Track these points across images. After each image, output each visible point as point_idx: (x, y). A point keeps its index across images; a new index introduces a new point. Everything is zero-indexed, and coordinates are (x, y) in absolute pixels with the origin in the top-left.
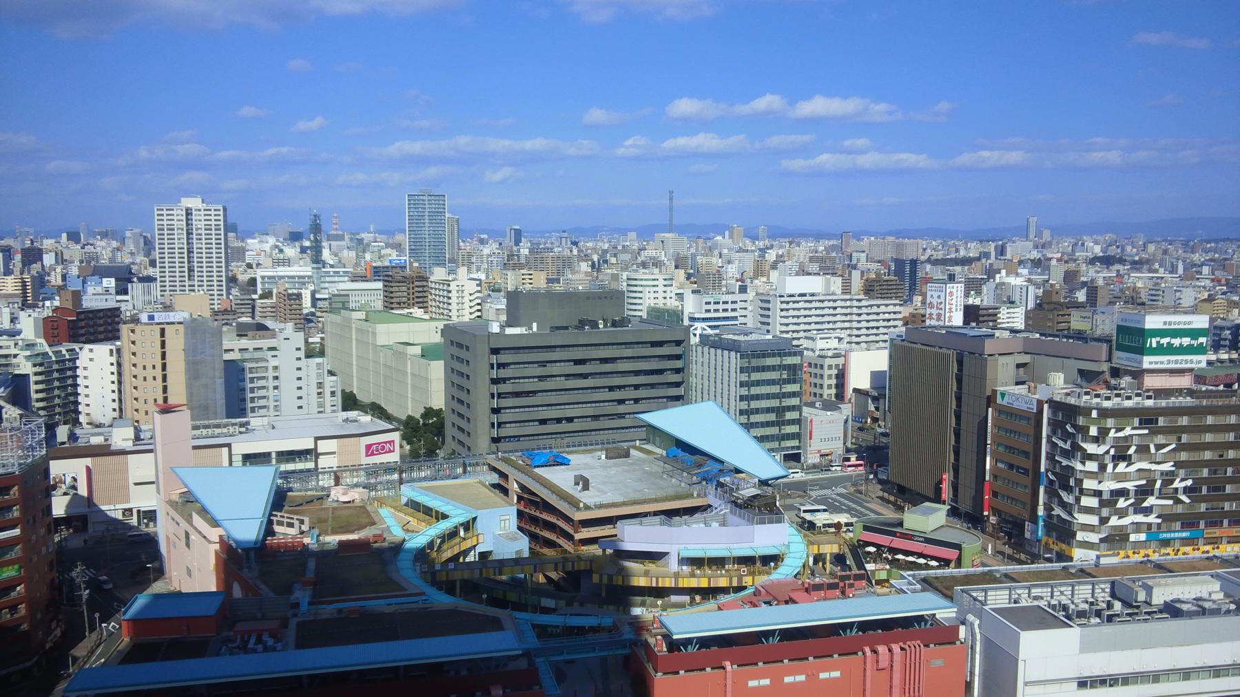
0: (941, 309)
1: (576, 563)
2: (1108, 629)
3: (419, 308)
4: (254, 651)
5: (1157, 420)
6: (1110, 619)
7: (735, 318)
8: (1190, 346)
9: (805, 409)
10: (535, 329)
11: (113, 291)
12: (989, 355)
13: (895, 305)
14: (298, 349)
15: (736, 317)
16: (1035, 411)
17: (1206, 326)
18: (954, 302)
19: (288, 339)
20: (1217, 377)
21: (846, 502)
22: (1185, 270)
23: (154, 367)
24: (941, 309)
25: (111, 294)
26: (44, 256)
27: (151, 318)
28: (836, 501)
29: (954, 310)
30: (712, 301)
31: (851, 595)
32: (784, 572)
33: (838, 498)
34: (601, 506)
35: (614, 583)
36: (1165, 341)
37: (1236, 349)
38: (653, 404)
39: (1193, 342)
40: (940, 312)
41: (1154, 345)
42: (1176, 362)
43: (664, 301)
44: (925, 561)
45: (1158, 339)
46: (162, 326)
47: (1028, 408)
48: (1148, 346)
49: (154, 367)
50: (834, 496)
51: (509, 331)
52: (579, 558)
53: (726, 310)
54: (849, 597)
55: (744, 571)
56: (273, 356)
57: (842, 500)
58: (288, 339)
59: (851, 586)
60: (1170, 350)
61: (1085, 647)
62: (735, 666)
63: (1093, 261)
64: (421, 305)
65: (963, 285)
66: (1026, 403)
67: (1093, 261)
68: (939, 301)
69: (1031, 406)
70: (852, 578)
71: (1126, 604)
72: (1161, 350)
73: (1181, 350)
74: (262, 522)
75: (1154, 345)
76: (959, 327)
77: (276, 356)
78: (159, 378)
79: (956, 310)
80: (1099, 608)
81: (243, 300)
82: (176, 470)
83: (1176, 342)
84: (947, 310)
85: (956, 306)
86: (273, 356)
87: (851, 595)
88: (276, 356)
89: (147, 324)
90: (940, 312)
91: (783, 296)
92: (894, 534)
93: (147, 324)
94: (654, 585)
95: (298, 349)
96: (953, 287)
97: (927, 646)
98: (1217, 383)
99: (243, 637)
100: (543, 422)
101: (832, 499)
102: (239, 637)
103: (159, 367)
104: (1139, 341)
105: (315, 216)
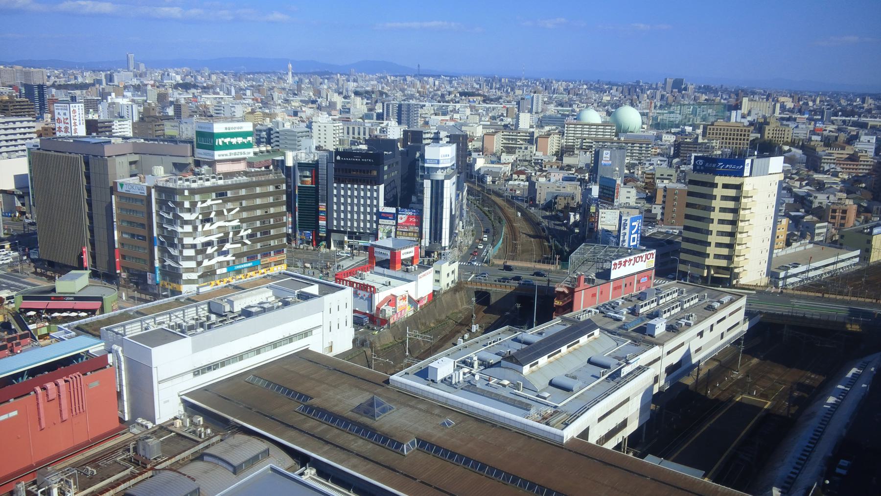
0: (68, 123)
2: (209, 333)
5: (226, 193)
12: (109, 157)
16: (146, 195)
24: (68, 123)
29: (78, 124)
39: (244, 140)
40: (67, 125)
41: (221, 143)
42: (235, 154)
45: (223, 139)
47: (140, 193)
60: (230, 146)
63: (176, 86)
69: (143, 191)
71: (219, 315)
72: (226, 147)
83: (234, 141)
84: (72, 124)
85: (80, 120)
90: (67, 125)
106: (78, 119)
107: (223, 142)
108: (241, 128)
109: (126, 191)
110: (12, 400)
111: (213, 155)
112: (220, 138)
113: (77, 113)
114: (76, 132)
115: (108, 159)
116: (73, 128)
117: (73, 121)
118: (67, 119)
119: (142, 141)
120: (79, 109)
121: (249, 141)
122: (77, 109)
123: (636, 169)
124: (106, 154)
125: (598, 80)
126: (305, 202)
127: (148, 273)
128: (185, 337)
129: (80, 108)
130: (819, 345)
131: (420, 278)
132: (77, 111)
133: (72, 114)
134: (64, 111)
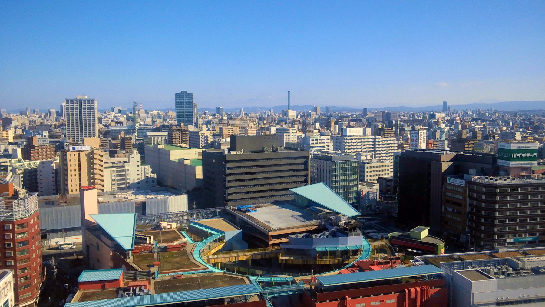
0: (417, 142)
1: (270, 254)
2: (508, 280)
3: (184, 143)
4: (139, 295)
5: (517, 189)
6: (509, 275)
7: (324, 147)
8: (530, 157)
9: (360, 186)
10: (243, 152)
11: (47, 137)
12: (443, 162)
13: (394, 140)
14: (138, 162)
15: (325, 146)
16: (464, 186)
17: (303, 168)
18: (422, 139)
19: (134, 157)
20: (539, 170)
21: (380, 226)
22: (513, 124)
23: (75, 170)
24: (417, 142)
25: (47, 138)
26: (12, 122)
27: (74, 148)
28: (375, 226)
29: (422, 142)
30: (314, 139)
31: (395, 267)
32: (360, 258)
33: (376, 225)
34: (279, 230)
35: (288, 263)
36: (519, 155)
37: (542, 159)
38: (294, 185)
39: (531, 155)
40: (417, 143)
41: (515, 157)
42: (521, 164)
43: (292, 139)
44: (413, 251)
45: (516, 154)
46: (79, 152)
47: (461, 184)
48: (512, 157)
49: (75, 170)
50: (374, 224)
51: (233, 153)
52: (237, 252)
53: (320, 143)
54: (394, 268)
55: (344, 257)
56: (127, 165)
57: (378, 226)
58: (134, 157)
59: (395, 263)
60: (522, 159)
61: (499, 288)
62: (350, 298)
63: (473, 120)
64: (185, 142)
65: (425, 131)
66: (460, 182)
67: (473, 120)
68: (416, 138)
69: (462, 184)
70: (395, 259)
71: (514, 269)
72: (518, 159)
73: (526, 159)
74: (133, 238)
75: (515, 157)
76: (520, 140)
77: (128, 165)
78: (78, 175)
79: (423, 142)
80: (503, 270)
81: (104, 140)
82: (91, 215)
83: (524, 155)
84: (419, 142)
85: (423, 140)
86: (127, 165)
87: (395, 267)
88: (128, 165)
89: (72, 151)
90: (417, 143)
91: (108, 163)
92: (406, 240)
93: (72, 151)
94: (306, 263)
95: (138, 162)
96: (422, 132)
97: (431, 288)
98: (539, 173)
99: (133, 289)
100: (247, 193)
101: (374, 225)
102: (131, 288)
103: (77, 170)
104: (508, 155)
105: (135, 103)
106: (422, 140)
107: (516, 155)
108: (530, 147)
109: (452, 183)
110: (372, 296)
111: (509, 164)
112: (515, 153)
113: (422, 136)
114: (421, 147)
115: (443, 163)
116: (419, 144)
117: (419, 141)
118: (417, 139)
119: (462, 153)
120: (423, 134)
121: (535, 156)
122: (422, 134)
123: (139, 121)
124: (441, 160)
125: (445, 103)
126: (81, 131)
127: (461, 235)
128: (265, 221)
129: (424, 133)
130: (455, 239)
131: (88, 151)
132: (422, 135)
133: (419, 137)
134: (416, 135)
